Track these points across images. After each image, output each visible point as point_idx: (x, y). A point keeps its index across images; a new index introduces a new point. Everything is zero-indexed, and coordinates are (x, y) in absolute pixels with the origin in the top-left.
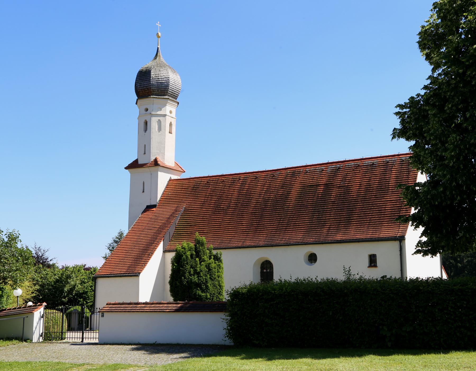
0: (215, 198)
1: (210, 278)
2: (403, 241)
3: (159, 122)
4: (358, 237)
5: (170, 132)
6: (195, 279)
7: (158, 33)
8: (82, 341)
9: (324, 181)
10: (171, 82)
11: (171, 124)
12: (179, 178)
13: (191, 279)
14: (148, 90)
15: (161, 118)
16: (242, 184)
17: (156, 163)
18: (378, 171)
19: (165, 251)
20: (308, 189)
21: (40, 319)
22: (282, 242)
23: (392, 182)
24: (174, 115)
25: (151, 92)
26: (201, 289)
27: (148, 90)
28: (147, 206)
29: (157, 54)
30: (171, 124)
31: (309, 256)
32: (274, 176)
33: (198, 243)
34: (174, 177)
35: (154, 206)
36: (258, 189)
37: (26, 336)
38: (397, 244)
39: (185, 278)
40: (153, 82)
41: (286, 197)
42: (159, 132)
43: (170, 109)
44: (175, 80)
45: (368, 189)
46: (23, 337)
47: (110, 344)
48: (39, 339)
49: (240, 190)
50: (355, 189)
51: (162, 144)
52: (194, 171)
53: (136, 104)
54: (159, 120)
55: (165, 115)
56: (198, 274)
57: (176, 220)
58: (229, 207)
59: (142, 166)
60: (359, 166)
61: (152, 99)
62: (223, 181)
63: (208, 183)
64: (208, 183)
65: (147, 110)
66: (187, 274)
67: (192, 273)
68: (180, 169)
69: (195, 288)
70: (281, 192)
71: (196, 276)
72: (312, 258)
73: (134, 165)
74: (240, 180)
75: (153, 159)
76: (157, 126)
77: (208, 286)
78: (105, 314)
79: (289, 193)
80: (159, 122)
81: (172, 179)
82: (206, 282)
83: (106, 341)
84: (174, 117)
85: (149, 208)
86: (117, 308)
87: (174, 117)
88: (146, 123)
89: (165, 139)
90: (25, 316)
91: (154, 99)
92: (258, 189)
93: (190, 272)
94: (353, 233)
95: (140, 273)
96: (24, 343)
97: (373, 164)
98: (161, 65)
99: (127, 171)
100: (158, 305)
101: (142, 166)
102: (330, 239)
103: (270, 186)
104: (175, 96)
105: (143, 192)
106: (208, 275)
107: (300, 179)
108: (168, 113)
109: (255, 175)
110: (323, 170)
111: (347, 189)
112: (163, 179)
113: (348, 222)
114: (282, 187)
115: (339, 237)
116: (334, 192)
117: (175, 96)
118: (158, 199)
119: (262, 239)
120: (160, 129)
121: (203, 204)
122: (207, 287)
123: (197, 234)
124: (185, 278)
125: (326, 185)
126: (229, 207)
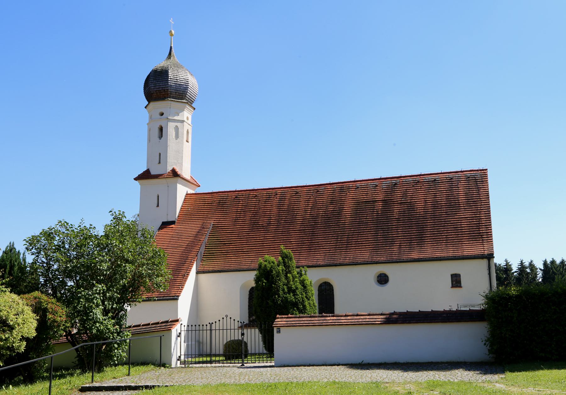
0: (249, 215)
1: (306, 297)
2: (491, 259)
3: (177, 128)
4: (438, 255)
5: (187, 141)
6: (291, 297)
7: (171, 31)
8: (243, 365)
9: (381, 197)
10: (190, 85)
11: (188, 132)
12: (194, 192)
13: (286, 298)
14: (165, 92)
15: (179, 124)
16: (280, 200)
17: (175, 174)
18: (443, 187)
19: (198, 273)
20: (361, 207)
21: (177, 339)
22: (347, 261)
23: (462, 199)
24: (190, 122)
25: (168, 94)
26: (298, 308)
27: (165, 92)
28: (163, 222)
29: (170, 53)
30: (188, 132)
31: (378, 277)
32: (318, 191)
33: (285, 257)
34: (191, 191)
35: (173, 223)
36: (302, 205)
37: (163, 360)
38: (485, 261)
39: (279, 297)
40: (171, 83)
41: (339, 213)
42: (176, 139)
43: (187, 114)
44: (193, 83)
45: (436, 205)
46: (162, 364)
47: (305, 366)
48: (176, 364)
49: (280, 206)
50: (420, 206)
51: (180, 152)
52: (209, 186)
53: (146, 107)
54: (177, 126)
55: (183, 121)
56: (294, 292)
57: (205, 239)
58: (269, 224)
59: (157, 177)
60: (418, 182)
61: (170, 102)
62: (256, 196)
63: (236, 197)
64: (236, 197)
65: (162, 114)
66: (281, 292)
67: (286, 290)
68: (195, 183)
69: (291, 308)
70: (331, 208)
71: (292, 294)
72: (383, 279)
73: (146, 176)
74: (277, 195)
75: (169, 169)
76: (174, 133)
77: (305, 306)
78: (282, 329)
79: (341, 209)
80: (177, 128)
81: (189, 193)
82: (303, 301)
83: (286, 364)
84: (190, 123)
85: (165, 225)
86: (305, 322)
87: (190, 123)
88: (161, 129)
89: (182, 147)
90: (161, 334)
91: (172, 102)
92: (302, 205)
93: (283, 290)
94: (429, 252)
95: (178, 296)
96: (162, 368)
97: (435, 180)
98: (178, 66)
99: (137, 182)
100: (355, 317)
101: (157, 177)
102: (405, 257)
103: (315, 202)
104: (190, 102)
105: (158, 206)
106: (304, 293)
107: (351, 195)
108: (185, 119)
109: (296, 191)
110: (377, 186)
111: (411, 206)
112: (182, 191)
113: (421, 240)
114: (331, 203)
115: (415, 255)
116: (396, 209)
117: (190, 102)
118: (177, 215)
119: (320, 259)
120: (177, 136)
121: (236, 220)
122: (304, 306)
123: (282, 247)
124: (279, 297)
125: (384, 201)
126: (269, 224)
